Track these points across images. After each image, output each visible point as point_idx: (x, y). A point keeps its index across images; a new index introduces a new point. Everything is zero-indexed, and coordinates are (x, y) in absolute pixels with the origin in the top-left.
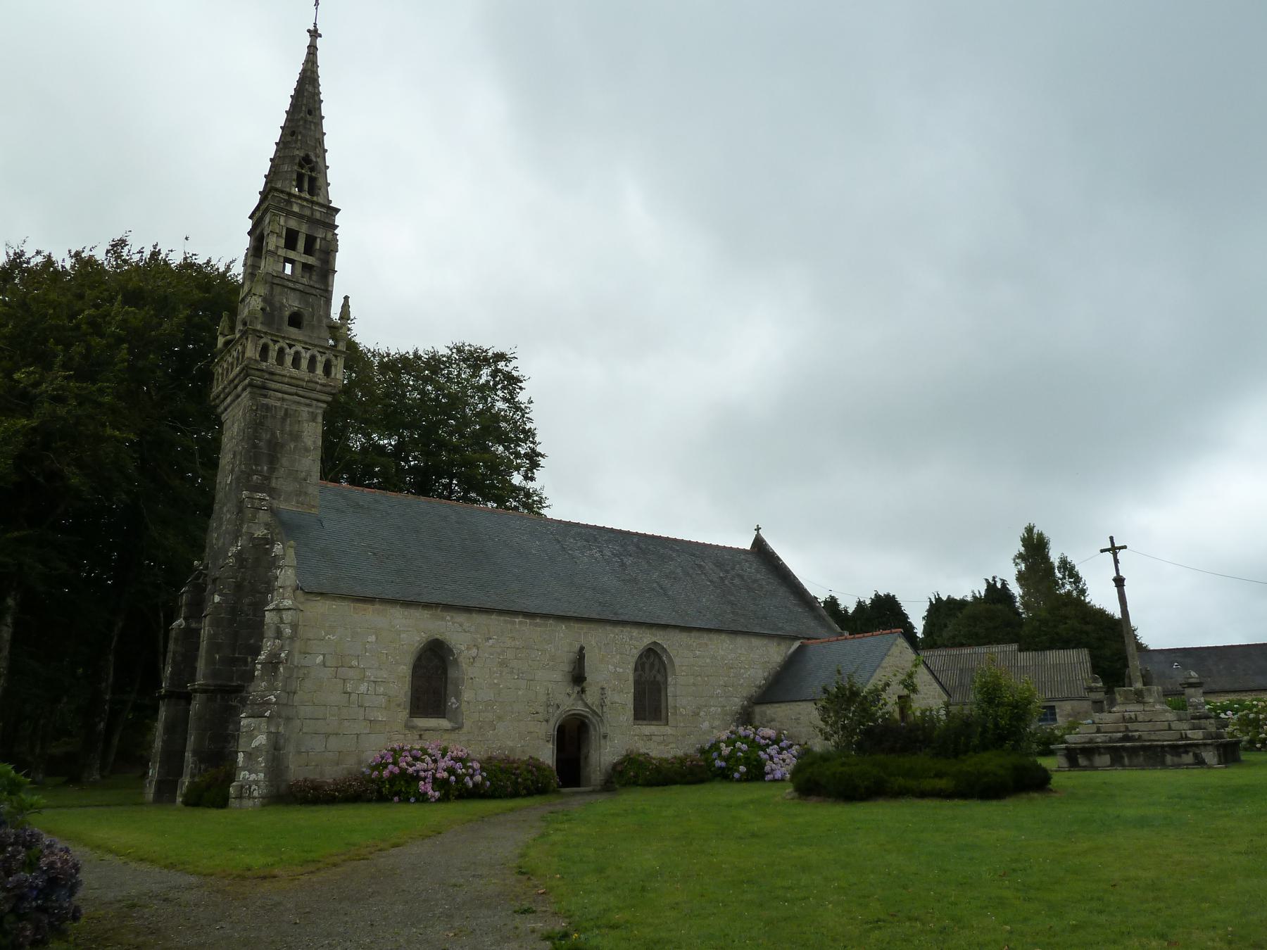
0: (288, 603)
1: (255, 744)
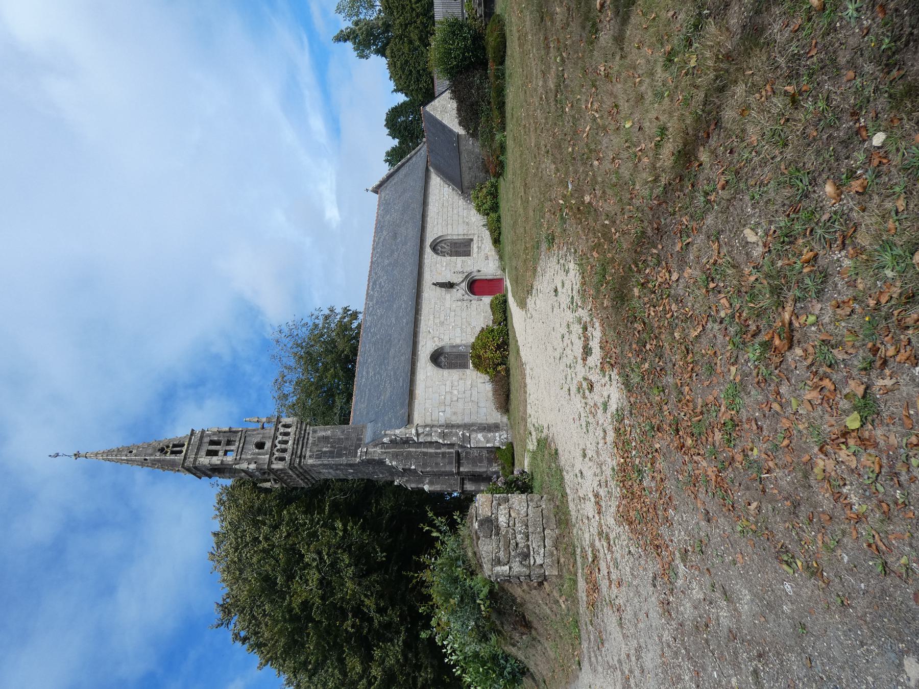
0: (414, 431)
1: (482, 439)
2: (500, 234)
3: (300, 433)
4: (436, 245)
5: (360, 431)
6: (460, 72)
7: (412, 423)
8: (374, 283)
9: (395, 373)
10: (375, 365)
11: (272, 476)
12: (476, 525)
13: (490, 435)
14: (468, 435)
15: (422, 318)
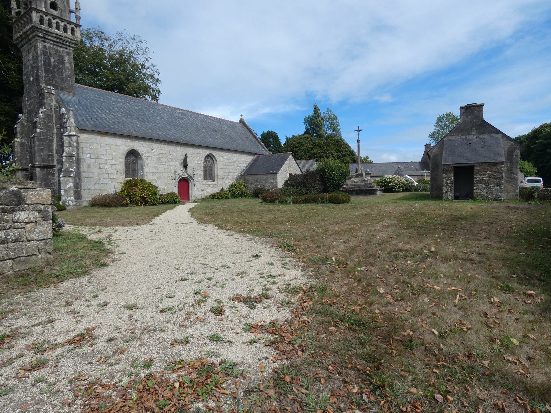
0: (73, 133)
1: (68, 186)
2: (219, 199)
3: (67, 41)
4: (211, 157)
5: (70, 90)
6: (321, 177)
7: (80, 133)
8: (184, 114)
9: (120, 123)
10: (126, 109)
11: (23, 11)
12: (14, 188)
13: (72, 192)
14: (72, 175)
15: (163, 145)
